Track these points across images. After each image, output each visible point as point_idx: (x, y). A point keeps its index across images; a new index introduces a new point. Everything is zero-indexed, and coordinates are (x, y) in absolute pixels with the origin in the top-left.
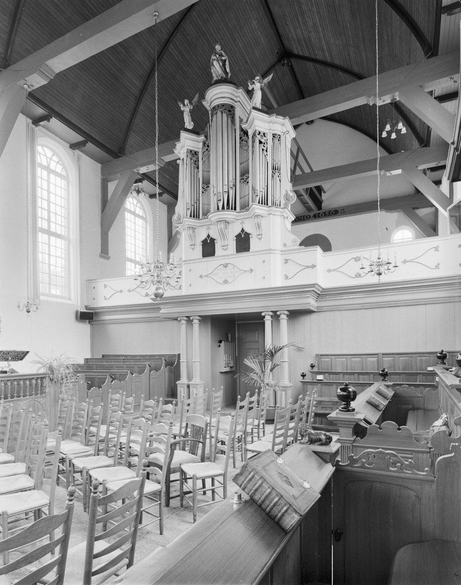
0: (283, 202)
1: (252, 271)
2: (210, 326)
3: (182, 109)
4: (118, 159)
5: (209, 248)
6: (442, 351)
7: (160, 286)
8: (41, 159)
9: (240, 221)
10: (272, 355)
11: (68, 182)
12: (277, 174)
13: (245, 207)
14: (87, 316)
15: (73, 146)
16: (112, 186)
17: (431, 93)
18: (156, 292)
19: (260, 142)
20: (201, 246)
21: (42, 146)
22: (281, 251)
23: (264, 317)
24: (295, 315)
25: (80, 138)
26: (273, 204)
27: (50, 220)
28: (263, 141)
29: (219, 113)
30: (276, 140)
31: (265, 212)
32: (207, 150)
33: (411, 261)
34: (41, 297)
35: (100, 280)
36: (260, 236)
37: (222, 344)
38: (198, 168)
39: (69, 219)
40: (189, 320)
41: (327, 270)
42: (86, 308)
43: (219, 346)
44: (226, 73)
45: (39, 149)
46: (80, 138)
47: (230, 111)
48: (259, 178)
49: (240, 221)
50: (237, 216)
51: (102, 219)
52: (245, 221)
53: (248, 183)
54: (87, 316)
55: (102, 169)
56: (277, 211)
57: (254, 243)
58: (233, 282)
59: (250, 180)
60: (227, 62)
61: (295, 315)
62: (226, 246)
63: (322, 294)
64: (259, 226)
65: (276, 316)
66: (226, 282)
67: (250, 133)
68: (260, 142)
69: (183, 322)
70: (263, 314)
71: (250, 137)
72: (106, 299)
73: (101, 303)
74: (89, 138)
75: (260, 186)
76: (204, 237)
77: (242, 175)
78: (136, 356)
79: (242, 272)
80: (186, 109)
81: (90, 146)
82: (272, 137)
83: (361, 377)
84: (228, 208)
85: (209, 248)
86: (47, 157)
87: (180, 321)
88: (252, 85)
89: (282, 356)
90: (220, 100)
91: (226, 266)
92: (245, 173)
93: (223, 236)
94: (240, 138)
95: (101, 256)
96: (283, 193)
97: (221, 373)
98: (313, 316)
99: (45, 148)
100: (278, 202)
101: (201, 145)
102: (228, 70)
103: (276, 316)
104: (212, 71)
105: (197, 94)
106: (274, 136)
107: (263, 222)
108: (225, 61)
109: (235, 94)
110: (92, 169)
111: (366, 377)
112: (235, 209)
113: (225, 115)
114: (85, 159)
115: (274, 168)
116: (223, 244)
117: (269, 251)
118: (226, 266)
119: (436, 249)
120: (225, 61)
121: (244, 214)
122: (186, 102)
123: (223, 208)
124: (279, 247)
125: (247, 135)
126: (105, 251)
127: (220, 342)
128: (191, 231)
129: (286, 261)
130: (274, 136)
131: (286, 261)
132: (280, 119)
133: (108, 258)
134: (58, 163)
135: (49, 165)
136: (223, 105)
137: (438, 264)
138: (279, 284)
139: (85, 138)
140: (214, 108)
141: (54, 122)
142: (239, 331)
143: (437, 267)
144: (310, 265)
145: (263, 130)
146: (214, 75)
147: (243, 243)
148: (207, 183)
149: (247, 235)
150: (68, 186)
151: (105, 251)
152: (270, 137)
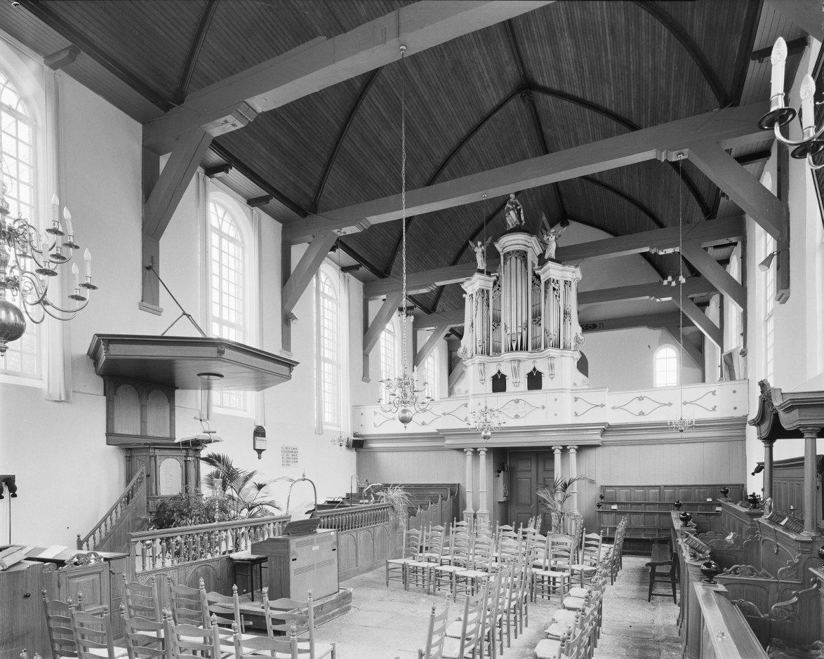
0: (573, 344)
1: (543, 407)
2: (492, 460)
3: (476, 250)
4: (385, 279)
5: (499, 383)
6: (754, 493)
7: (408, 408)
8: (213, 220)
9: (532, 360)
10: (565, 486)
11: (243, 248)
12: (568, 318)
13: (536, 347)
14: (358, 444)
15: (252, 202)
16: (298, 252)
17: (692, 299)
18: (403, 415)
19: (554, 289)
20: (491, 382)
21: (215, 203)
22: (572, 390)
23: (554, 451)
24: (581, 448)
25: (261, 192)
26: (565, 348)
27: (222, 303)
28: (556, 288)
29: (513, 259)
30: (567, 287)
31: (557, 354)
32: (498, 289)
33: (691, 403)
34: (324, 426)
35: (369, 407)
36: (552, 376)
37: (502, 474)
38: (489, 306)
39: (38, 208)
40: (476, 452)
41: (615, 407)
42: (355, 435)
43: (499, 476)
44: (521, 221)
45: (211, 207)
46: (261, 192)
47: (524, 257)
48: (551, 320)
49: (532, 360)
50: (530, 356)
51: (364, 340)
52: (537, 360)
53: (540, 325)
54: (358, 444)
55: (364, 288)
56: (568, 353)
57: (545, 381)
58: (522, 415)
59: (542, 322)
60: (522, 211)
61: (581, 448)
62: (517, 384)
63: (607, 429)
64: (552, 367)
65: (565, 450)
66: (517, 417)
67: (542, 277)
68: (554, 289)
69: (469, 453)
70: (553, 448)
71: (543, 282)
72: (375, 426)
73: (369, 430)
74: (274, 192)
75: (553, 329)
76: (494, 372)
77: (534, 317)
78: (422, 485)
79: (533, 408)
80: (479, 251)
81: (275, 203)
82: (564, 283)
83: (647, 507)
84: (521, 349)
85: (499, 383)
86: (218, 217)
87: (466, 452)
88: (547, 236)
89: (573, 489)
90: (513, 246)
91: (517, 401)
92: (537, 316)
93: (515, 372)
94: (533, 282)
95: (142, 307)
96: (574, 336)
97: (499, 502)
98: (598, 450)
99: (218, 207)
100: (568, 345)
101: (491, 284)
102: (522, 218)
103: (565, 450)
104: (507, 218)
105: (490, 238)
106: (566, 282)
107: (556, 362)
108: (520, 209)
109: (529, 240)
110: (273, 229)
111: (651, 507)
112: (527, 350)
113: (519, 261)
114: (266, 218)
115: (565, 313)
116: (515, 380)
117: (562, 390)
118: (517, 401)
119: (714, 393)
120: (520, 209)
121: (537, 354)
122: (479, 243)
123: (517, 349)
124: (569, 386)
125: (540, 280)
126: (365, 376)
127: (499, 472)
128: (482, 367)
129: (576, 399)
130: (566, 282)
131: (576, 399)
132: (572, 268)
133: (368, 381)
134: (330, 286)
135: (221, 227)
136: (518, 251)
137: (715, 407)
138: (569, 422)
139: (267, 192)
140: (508, 253)
141: (234, 174)
142: (510, 460)
143: (714, 409)
144: (600, 404)
145: (556, 278)
146: (509, 222)
147: (535, 380)
148: (497, 320)
149: (539, 375)
150: (35, 138)
151: (365, 376)
152: (562, 283)
